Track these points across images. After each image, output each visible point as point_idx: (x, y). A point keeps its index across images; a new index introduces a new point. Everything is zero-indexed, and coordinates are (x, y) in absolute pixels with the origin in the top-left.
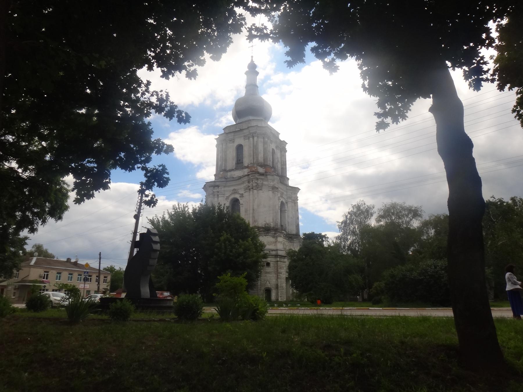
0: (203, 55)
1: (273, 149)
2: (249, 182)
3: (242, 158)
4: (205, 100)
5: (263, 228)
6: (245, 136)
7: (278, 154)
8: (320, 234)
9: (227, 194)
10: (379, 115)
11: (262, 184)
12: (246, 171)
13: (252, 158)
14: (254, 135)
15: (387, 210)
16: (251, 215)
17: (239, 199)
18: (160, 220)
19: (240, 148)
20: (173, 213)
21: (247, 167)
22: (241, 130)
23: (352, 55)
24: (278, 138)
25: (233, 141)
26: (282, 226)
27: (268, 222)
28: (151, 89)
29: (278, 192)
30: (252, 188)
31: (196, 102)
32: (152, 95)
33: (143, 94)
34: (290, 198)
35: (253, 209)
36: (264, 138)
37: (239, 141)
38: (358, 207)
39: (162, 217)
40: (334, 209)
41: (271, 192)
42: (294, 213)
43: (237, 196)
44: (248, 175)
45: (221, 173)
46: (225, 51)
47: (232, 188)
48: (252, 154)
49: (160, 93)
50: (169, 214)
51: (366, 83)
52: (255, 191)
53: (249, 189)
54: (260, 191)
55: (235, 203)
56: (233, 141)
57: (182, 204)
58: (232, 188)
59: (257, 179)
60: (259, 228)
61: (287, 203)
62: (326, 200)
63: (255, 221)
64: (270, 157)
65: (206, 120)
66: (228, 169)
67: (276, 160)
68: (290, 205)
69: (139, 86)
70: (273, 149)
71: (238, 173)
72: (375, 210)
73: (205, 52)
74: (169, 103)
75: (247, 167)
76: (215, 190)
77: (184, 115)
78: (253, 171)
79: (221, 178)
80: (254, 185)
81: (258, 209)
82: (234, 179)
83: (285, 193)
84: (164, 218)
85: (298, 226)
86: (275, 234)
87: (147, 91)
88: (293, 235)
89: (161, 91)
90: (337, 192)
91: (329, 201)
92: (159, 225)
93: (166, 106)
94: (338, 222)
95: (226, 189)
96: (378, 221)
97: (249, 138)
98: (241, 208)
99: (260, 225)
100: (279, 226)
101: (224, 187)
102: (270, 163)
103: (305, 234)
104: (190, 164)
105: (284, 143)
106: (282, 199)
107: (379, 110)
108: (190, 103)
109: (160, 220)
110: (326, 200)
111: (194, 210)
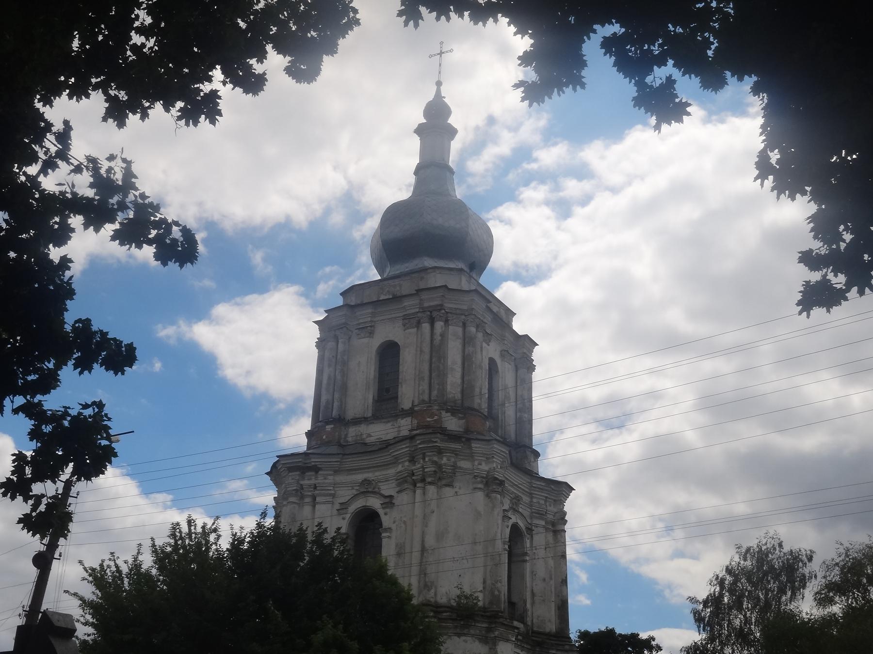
0: (262, 56)
1: (492, 361)
2: (412, 460)
3: (396, 382)
4: (328, 211)
5: (450, 608)
6: (406, 318)
7: (507, 375)
8: (634, 636)
9: (344, 494)
10: (808, 259)
11: (455, 467)
12: (405, 425)
13: (425, 386)
14: (435, 314)
15: (850, 569)
16: (415, 570)
17: (381, 512)
18: (125, 569)
19: (389, 353)
20: (169, 549)
21: (410, 413)
22: (397, 299)
23: (740, 75)
24: (508, 326)
25: (368, 330)
26: (511, 604)
27: (467, 590)
28: (79, 150)
29: (502, 494)
30: (423, 480)
31: (301, 217)
32: (78, 169)
33: (49, 165)
34: (541, 515)
35: (423, 550)
36: (464, 325)
37: (389, 330)
38: (761, 556)
39: (131, 561)
40: (695, 557)
41: (480, 495)
42: (551, 562)
43: (374, 503)
44: (411, 438)
45: (329, 428)
46: (332, 50)
47: (360, 477)
48: (427, 373)
49: (105, 165)
50: (155, 552)
51: (775, 156)
52: (432, 490)
53: (411, 482)
54: (448, 491)
55: (367, 524)
56: (368, 330)
57: (202, 520)
58: (360, 477)
59: (440, 452)
60: (437, 608)
61: (530, 530)
62: (669, 529)
63: (426, 586)
64: (482, 383)
65: (328, 269)
66: (350, 414)
67: (501, 395)
68: (540, 538)
69: (39, 139)
70: (492, 361)
71: (379, 431)
72: (815, 566)
73: (269, 48)
74: (131, 197)
75: (410, 413)
76: (306, 482)
77: (176, 232)
78: (427, 427)
79: (328, 443)
80: (430, 469)
81: (440, 546)
82: (365, 449)
83: (526, 499)
84: (136, 566)
85: (562, 608)
86: (489, 630)
87: (63, 155)
88: (549, 635)
89: (111, 158)
90: (707, 503)
91: (679, 534)
92: (119, 588)
93: (122, 206)
94: (692, 600)
95: (340, 478)
96: (823, 600)
97: (418, 324)
98: (385, 542)
99: (443, 600)
100: (503, 606)
101: (337, 472)
102: (481, 402)
103: (584, 635)
104: (264, 398)
105: (527, 343)
106: (514, 519)
107: (817, 246)
108: (282, 219)
109: (125, 569)
110: (669, 529)
111: (237, 542)
